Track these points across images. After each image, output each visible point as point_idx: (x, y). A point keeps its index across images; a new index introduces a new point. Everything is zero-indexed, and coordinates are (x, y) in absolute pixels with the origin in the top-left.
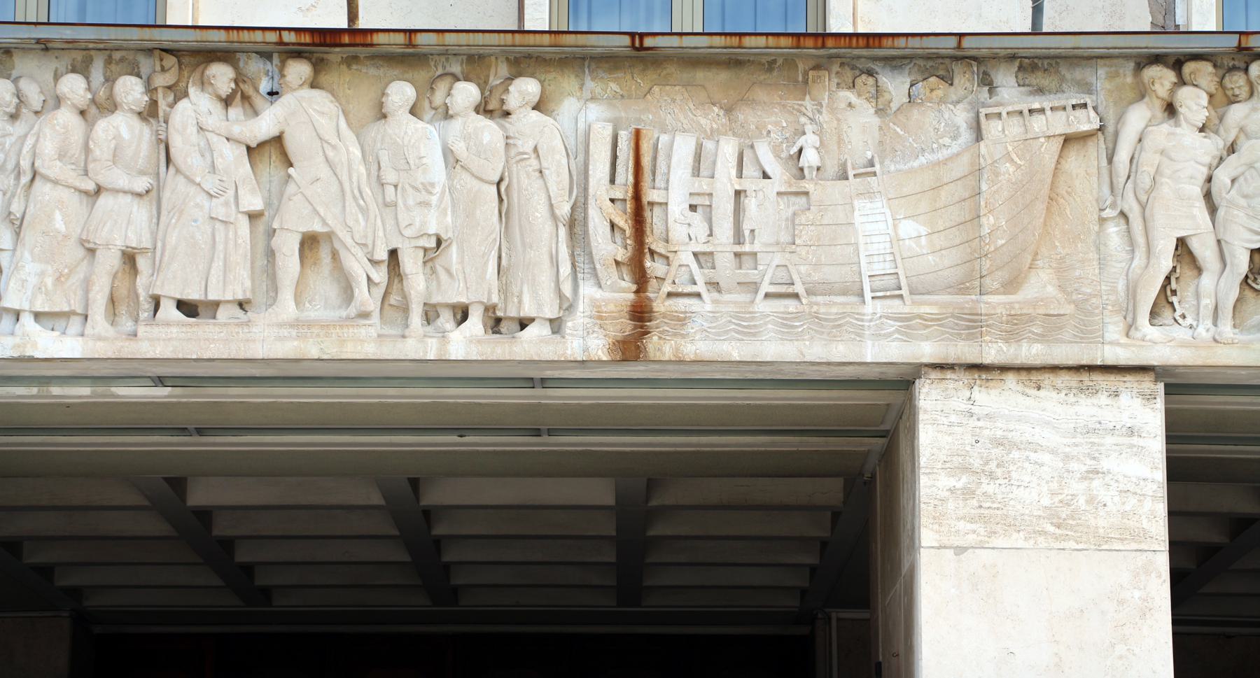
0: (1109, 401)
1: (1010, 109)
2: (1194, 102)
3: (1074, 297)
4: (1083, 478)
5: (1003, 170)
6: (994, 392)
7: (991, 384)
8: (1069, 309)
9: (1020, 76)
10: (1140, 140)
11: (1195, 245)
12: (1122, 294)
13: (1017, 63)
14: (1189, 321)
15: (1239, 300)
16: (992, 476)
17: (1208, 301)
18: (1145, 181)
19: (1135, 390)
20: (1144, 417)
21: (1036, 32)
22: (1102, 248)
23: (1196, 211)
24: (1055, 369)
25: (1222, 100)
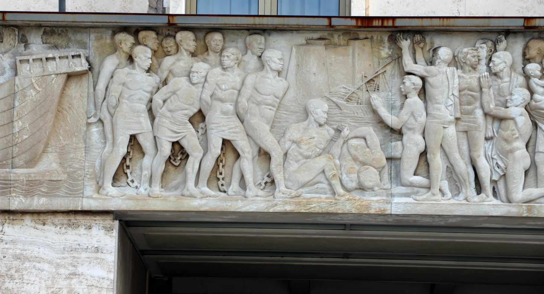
0: (85, 232)
1: (34, 57)
2: (144, 55)
3: (68, 170)
4: (67, 278)
5: (29, 93)
6: (16, 227)
7: (15, 222)
8: (64, 177)
9: (44, 37)
10: (112, 77)
11: (141, 139)
12: (98, 168)
13: (42, 30)
14: (136, 184)
15: (165, 172)
16: (12, 278)
17: (147, 172)
18: (114, 101)
19: (101, 225)
20: (106, 241)
21: (62, 11)
22: (87, 140)
23: (142, 119)
24: (54, 213)
25: (159, 54)
